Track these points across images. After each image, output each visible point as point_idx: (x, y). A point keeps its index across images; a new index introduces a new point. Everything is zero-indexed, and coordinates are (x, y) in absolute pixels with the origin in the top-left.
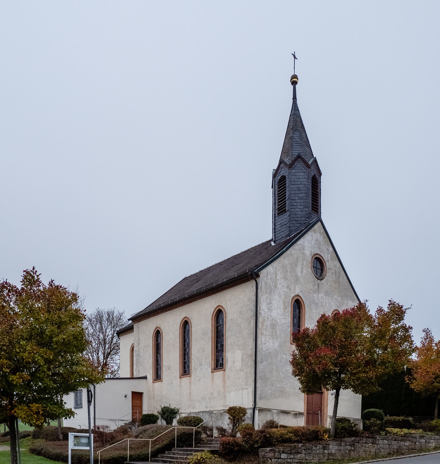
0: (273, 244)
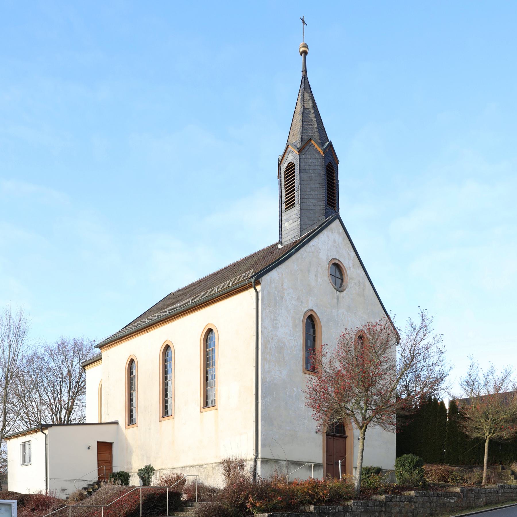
0: (280, 246)
